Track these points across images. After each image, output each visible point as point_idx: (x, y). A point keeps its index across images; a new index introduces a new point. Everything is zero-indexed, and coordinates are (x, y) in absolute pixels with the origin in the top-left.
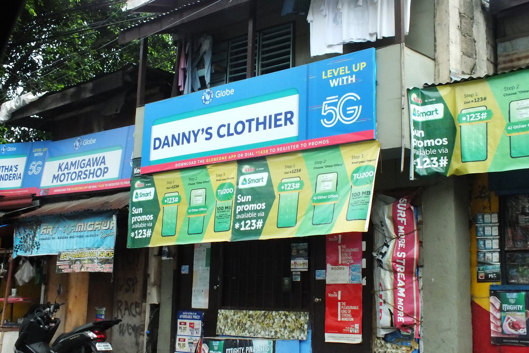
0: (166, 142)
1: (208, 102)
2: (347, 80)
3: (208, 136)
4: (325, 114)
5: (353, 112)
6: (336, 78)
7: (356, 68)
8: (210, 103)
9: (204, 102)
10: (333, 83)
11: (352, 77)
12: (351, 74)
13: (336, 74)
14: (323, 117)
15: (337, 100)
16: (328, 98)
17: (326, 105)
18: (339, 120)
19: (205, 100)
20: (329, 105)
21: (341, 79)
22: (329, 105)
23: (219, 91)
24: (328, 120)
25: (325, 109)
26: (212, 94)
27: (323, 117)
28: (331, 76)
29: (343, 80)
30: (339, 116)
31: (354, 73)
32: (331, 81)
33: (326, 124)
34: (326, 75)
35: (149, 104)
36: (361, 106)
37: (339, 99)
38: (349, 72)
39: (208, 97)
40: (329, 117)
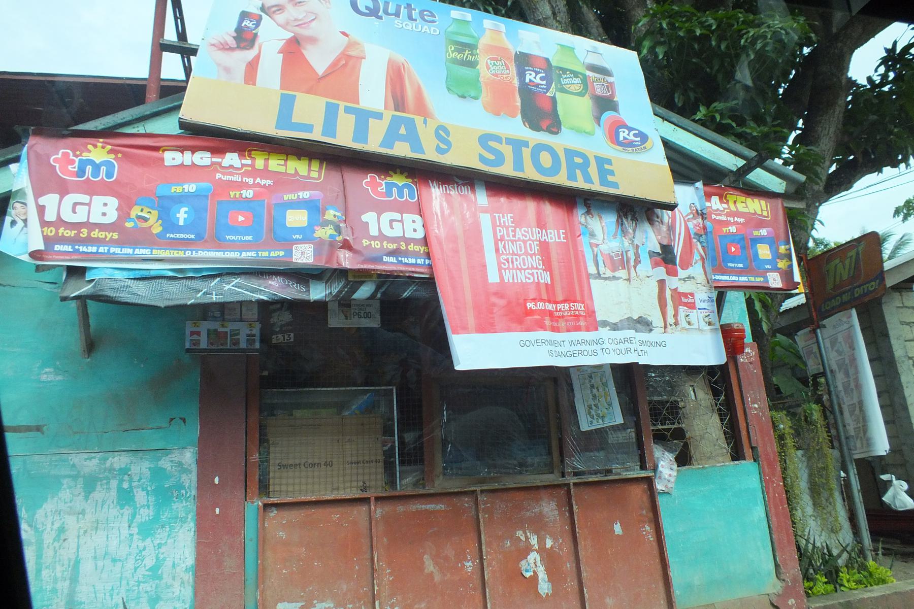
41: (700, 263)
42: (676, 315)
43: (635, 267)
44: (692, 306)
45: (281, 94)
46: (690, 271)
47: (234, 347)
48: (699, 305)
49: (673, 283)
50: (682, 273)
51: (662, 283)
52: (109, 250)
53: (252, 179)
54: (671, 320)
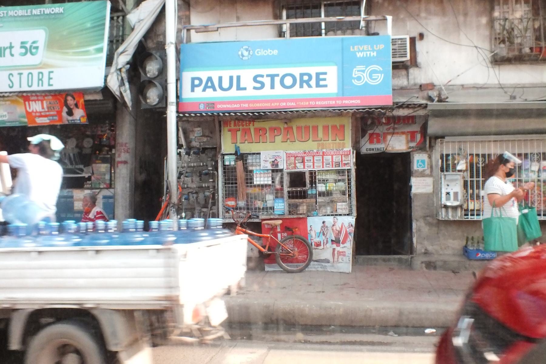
0: (209, 84)
1: (247, 58)
2: (370, 54)
3: (259, 85)
4: (356, 76)
5: (377, 77)
6: (361, 52)
7: (377, 48)
8: (248, 59)
9: (241, 57)
10: (359, 55)
11: (373, 53)
12: (373, 51)
13: (361, 49)
14: (354, 79)
15: (364, 69)
16: (357, 67)
17: (356, 71)
18: (366, 81)
19: (243, 56)
20: (358, 71)
21: (365, 53)
22: (358, 71)
23: (260, 50)
24: (358, 80)
25: (355, 73)
26: (251, 51)
27: (354, 79)
28: (358, 50)
29: (367, 54)
30: (366, 79)
31: (376, 50)
32: (357, 53)
33: (356, 82)
34: (353, 48)
35: (453, 109)
36: (383, 75)
37: (366, 68)
38: (371, 49)
39: (246, 53)
40: (359, 79)
41: (349, 242)
42: (338, 258)
43: (326, 245)
44: (344, 255)
45: (291, 36)
46: (345, 245)
47: (317, 180)
48: (347, 255)
49: (338, 249)
50: (342, 245)
51: (334, 249)
52: (271, 104)
53: (288, 105)
54: (336, 259)
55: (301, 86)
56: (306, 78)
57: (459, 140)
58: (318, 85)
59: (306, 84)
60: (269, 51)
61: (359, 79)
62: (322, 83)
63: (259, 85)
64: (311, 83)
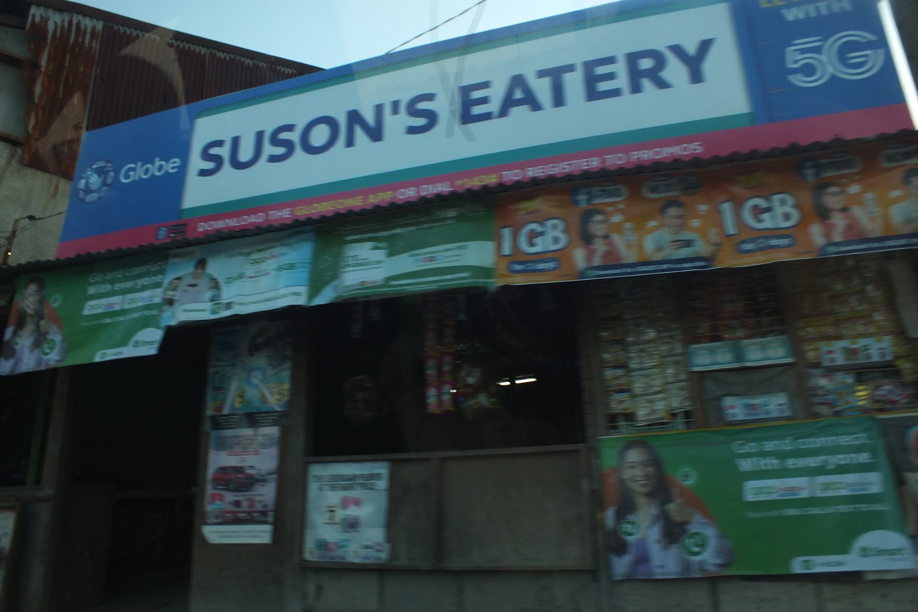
3: (421, 122)
20: (803, 51)
22: (803, 51)
25: (794, 57)
33: (799, 80)
40: (808, 70)
55: (636, 88)
56: (646, 64)
57: (195, 288)
58: (593, 94)
59: (790, 75)
60: (158, 163)
61: (808, 70)
62: (603, 86)
63: (421, 122)
64: (665, 74)
